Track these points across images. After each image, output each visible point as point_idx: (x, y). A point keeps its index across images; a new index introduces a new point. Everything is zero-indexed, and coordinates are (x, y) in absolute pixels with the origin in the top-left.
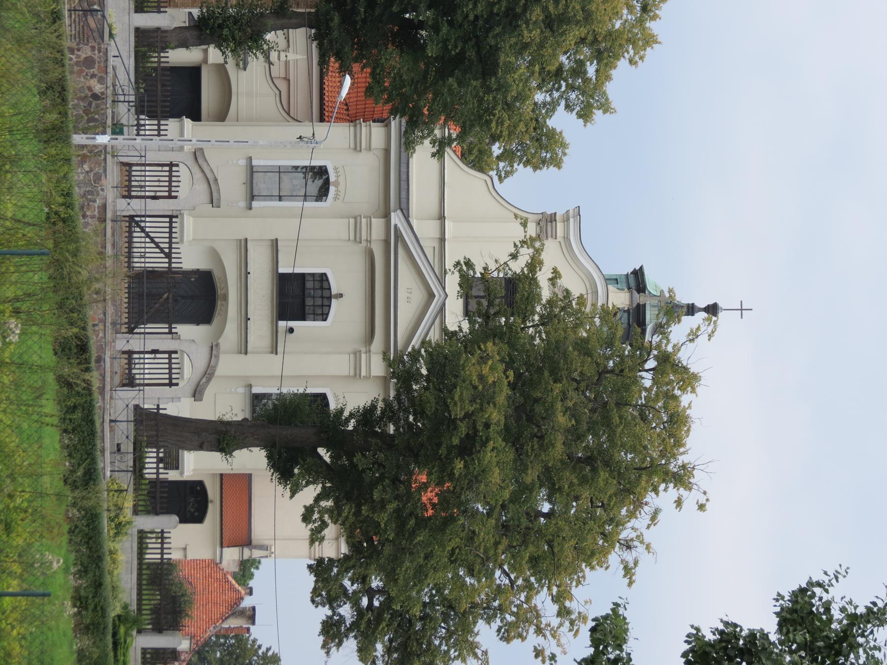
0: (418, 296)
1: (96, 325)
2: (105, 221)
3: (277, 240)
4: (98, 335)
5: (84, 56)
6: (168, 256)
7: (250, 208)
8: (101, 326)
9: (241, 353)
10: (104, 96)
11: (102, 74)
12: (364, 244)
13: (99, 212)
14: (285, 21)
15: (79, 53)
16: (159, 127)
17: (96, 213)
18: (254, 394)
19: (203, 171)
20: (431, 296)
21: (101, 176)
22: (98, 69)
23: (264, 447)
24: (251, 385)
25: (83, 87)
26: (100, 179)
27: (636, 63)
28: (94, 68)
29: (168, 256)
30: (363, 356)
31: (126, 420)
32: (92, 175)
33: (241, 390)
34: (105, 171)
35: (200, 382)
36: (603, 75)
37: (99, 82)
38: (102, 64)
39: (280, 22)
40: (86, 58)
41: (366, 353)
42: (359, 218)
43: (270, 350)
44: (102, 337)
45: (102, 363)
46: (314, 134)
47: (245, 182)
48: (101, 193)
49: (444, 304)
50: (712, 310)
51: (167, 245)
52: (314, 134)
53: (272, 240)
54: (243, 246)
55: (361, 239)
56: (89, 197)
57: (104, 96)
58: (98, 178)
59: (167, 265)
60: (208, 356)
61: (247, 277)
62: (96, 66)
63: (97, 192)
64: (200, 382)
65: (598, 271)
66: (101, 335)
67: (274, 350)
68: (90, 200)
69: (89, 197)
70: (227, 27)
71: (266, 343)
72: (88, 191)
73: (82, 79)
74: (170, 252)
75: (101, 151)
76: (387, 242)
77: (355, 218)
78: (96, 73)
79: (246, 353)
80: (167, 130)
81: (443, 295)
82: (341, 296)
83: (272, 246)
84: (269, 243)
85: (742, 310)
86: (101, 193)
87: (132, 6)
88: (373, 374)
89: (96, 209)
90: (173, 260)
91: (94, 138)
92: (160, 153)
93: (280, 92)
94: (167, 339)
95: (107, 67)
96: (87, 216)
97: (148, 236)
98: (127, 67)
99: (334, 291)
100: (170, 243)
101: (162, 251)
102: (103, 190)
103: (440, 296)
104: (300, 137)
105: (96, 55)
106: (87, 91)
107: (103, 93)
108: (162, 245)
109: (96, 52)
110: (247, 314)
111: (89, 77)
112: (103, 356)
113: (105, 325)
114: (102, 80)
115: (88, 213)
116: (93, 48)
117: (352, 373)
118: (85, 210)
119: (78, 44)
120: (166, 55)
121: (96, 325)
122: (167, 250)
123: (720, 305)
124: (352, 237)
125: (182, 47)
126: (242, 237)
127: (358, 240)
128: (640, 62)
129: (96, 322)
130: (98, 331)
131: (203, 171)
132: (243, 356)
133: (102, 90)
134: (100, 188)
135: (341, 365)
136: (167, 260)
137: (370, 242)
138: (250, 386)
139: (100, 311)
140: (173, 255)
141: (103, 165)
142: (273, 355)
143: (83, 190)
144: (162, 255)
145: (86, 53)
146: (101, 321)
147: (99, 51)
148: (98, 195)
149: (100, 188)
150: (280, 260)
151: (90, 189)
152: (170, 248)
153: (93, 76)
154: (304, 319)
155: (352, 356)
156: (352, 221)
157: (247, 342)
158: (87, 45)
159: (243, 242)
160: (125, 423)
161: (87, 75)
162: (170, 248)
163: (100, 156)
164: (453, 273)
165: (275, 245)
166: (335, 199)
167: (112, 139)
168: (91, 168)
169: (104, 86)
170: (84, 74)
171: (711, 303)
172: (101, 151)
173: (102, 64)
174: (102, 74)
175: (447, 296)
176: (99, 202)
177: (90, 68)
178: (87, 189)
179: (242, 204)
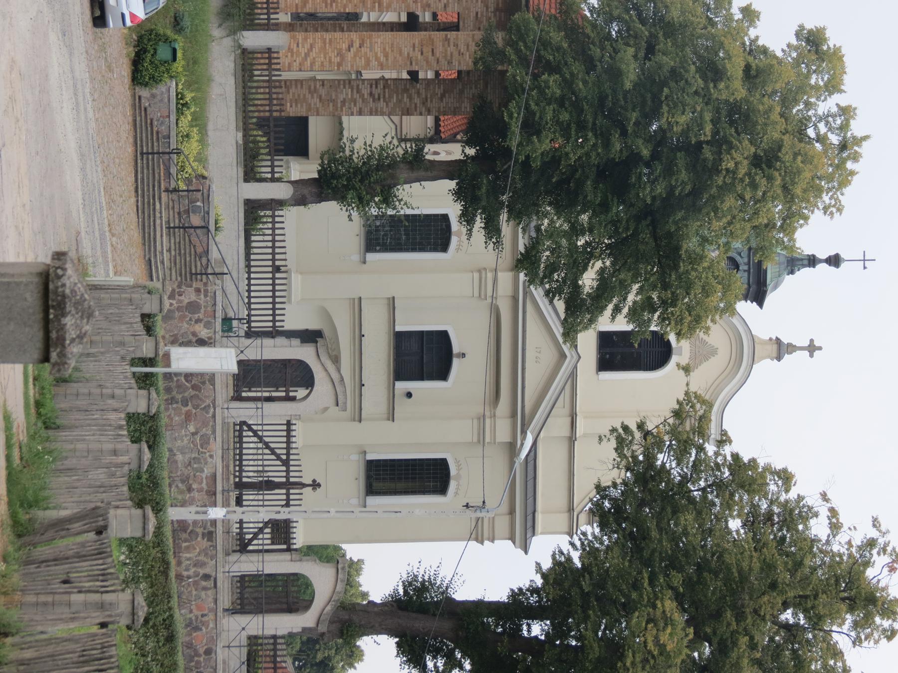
0: (549, 356)
1: (206, 615)
2: (215, 494)
3: (394, 298)
4: (208, 625)
5: (186, 301)
6: (286, 463)
7: (364, 262)
8: (211, 616)
9: (354, 420)
10: (212, 341)
11: (209, 319)
12: (489, 300)
13: (207, 484)
14: (422, 173)
15: (180, 298)
16: (274, 312)
17: (204, 485)
18: (368, 461)
19: (326, 370)
20: (563, 356)
21: (209, 439)
22: (205, 314)
23: (391, 633)
24: (365, 452)
25: (186, 333)
26: (208, 443)
27: (832, 214)
28: (199, 312)
29: (286, 463)
30: (488, 421)
31: (238, 645)
32: (198, 438)
33: (355, 457)
34: (214, 432)
35: (324, 610)
36: (792, 239)
37: (205, 326)
38: (209, 309)
39: (414, 175)
40: (189, 303)
41: (491, 417)
42: (484, 273)
43: (386, 416)
44: (212, 628)
45: (213, 655)
46: (484, 502)
47: (358, 233)
48: (209, 460)
49: (576, 367)
50: (834, 261)
51: (284, 451)
52: (484, 502)
53: (389, 299)
54: (357, 305)
55: (486, 296)
56: (195, 466)
57: (212, 341)
58: (205, 441)
59: (292, 491)
60: (333, 580)
61: (361, 341)
62: (202, 310)
63: (205, 459)
64: (324, 610)
65: (744, 325)
66: (211, 625)
67: (391, 417)
68: (197, 470)
69: (195, 466)
70: (354, 188)
71: (383, 408)
72: (194, 458)
73: (185, 325)
74: (288, 460)
75: (209, 406)
76: (515, 299)
77: (479, 271)
78: (201, 317)
79: (360, 421)
80: (283, 321)
81: (575, 356)
82: (464, 355)
83: (389, 305)
84: (386, 302)
85: (864, 260)
86: (209, 460)
87: (241, 174)
88: (498, 440)
89: (204, 481)
90: (292, 468)
91: (205, 513)
92: (276, 349)
93: (396, 126)
94: (285, 561)
95: (215, 311)
96: (194, 490)
97: (268, 447)
98: (237, 283)
99: (456, 350)
100: (288, 448)
101: (278, 457)
102: (211, 456)
103: (572, 356)
104: (467, 506)
105: (202, 299)
106: (191, 337)
107: (210, 338)
108: (278, 451)
109: (202, 296)
110: (361, 381)
111: (193, 323)
112: (214, 648)
113: (216, 615)
114: (208, 325)
115: (195, 486)
116: (198, 291)
117: (475, 440)
118: (191, 482)
119: (179, 286)
120: (281, 213)
121: (206, 615)
122: (284, 457)
123: (843, 256)
124: (476, 294)
125: (299, 205)
126: (356, 296)
127: (483, 297)
128: (837, 215)
129: (206, 612)
130: (208, 621)
131: (326, 370)
132: (357, 423)
133: (210, 335)
134: (208, 454)
135: (465, 431)
136: (284, 468)
137: (496, 298)
138: (365, 453)
139: (211, 599)
140: (292, 463)
141: (211, 423)
142: (390, 422)
143: (188, 456)
144: (279, 463)
145: (190, 298)
146: (210, 610)
147: (206, 296)
148: (206, 463)
149: (208, 454)
150: (396, 318)
151: (197, 455)
152: (288, 454)
153: (198, 321)
154: (421, 378)
155: (475, 421)
156: (476, 275)
157: (361, 409)
158: (191, 286)
159: (357, 302)
160: (238, 649)
161: (191, 320)
162: (288, 454)
163: (207, 413)
164: (609, 440)
165: (392, 303)
166: (458, 250)
167: (228, 512)
168: (197, 429)
169: (212, 330)
170: (188, 319)
171: (833, 253)
172: (209, 406)
173: (209, 309)
174: (209, 319)
175: (580, 357)
176: (207, 471)
177: (194, 313)
178: (193, 456)
179: (356, 257)
